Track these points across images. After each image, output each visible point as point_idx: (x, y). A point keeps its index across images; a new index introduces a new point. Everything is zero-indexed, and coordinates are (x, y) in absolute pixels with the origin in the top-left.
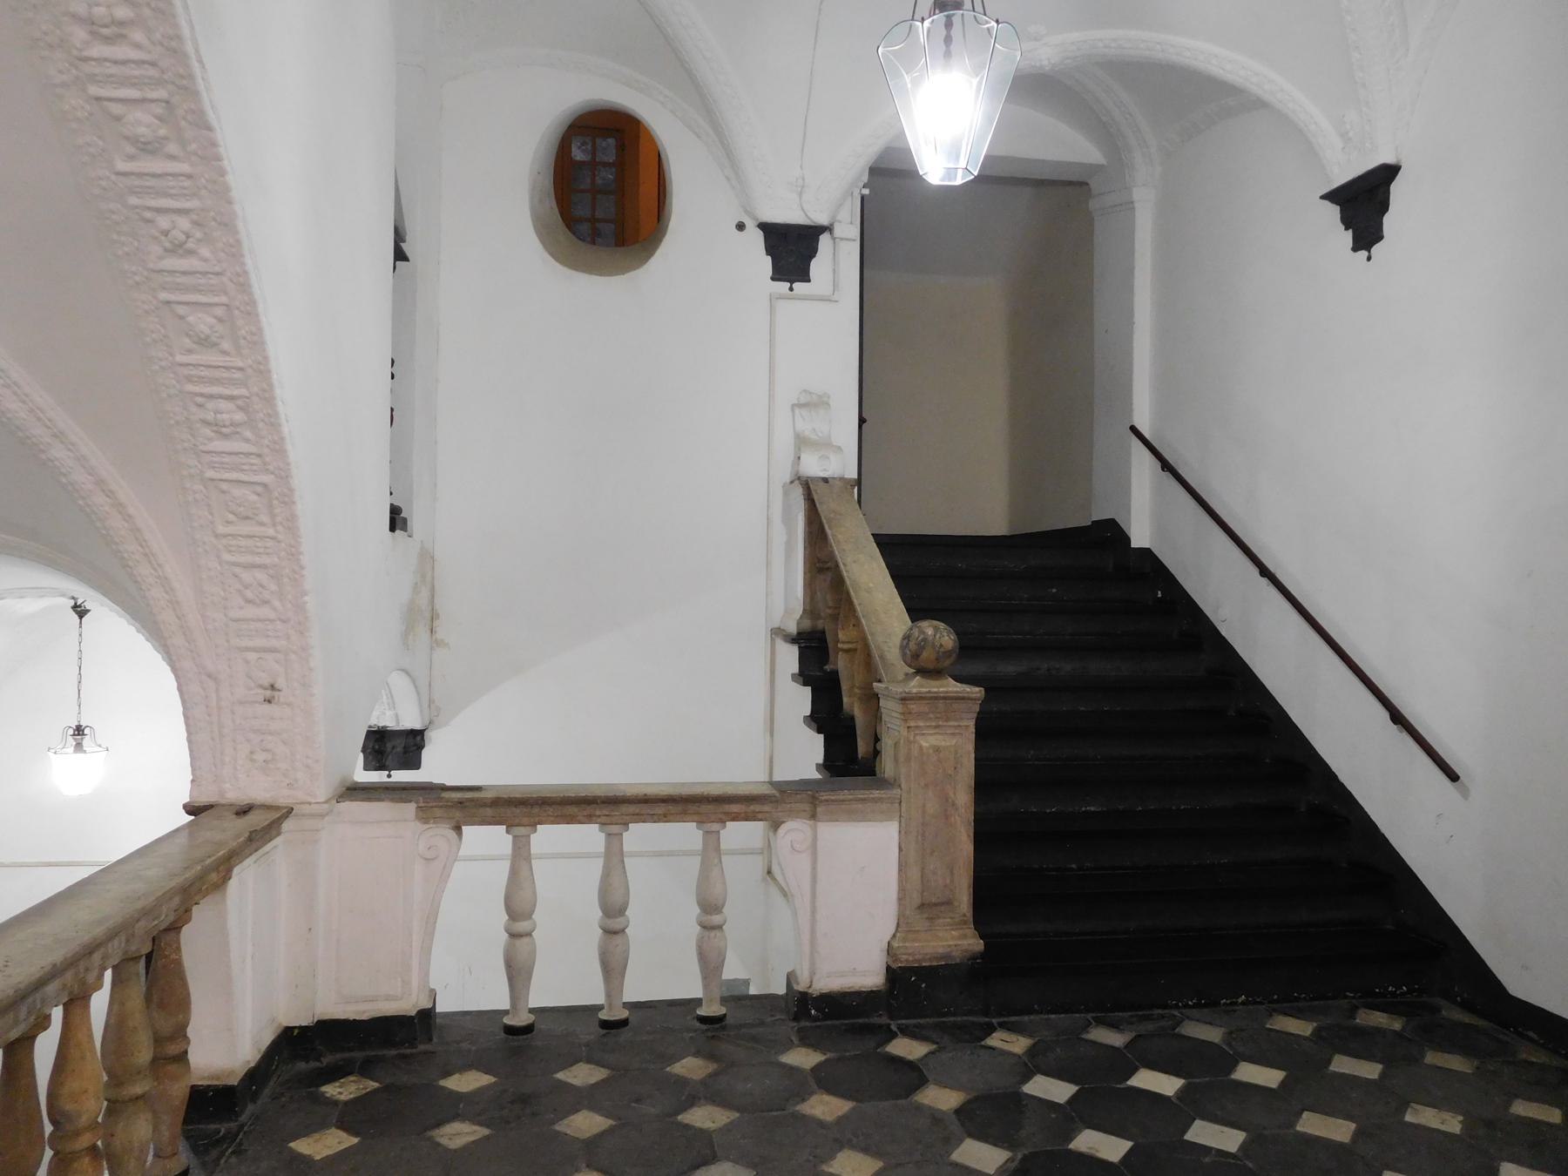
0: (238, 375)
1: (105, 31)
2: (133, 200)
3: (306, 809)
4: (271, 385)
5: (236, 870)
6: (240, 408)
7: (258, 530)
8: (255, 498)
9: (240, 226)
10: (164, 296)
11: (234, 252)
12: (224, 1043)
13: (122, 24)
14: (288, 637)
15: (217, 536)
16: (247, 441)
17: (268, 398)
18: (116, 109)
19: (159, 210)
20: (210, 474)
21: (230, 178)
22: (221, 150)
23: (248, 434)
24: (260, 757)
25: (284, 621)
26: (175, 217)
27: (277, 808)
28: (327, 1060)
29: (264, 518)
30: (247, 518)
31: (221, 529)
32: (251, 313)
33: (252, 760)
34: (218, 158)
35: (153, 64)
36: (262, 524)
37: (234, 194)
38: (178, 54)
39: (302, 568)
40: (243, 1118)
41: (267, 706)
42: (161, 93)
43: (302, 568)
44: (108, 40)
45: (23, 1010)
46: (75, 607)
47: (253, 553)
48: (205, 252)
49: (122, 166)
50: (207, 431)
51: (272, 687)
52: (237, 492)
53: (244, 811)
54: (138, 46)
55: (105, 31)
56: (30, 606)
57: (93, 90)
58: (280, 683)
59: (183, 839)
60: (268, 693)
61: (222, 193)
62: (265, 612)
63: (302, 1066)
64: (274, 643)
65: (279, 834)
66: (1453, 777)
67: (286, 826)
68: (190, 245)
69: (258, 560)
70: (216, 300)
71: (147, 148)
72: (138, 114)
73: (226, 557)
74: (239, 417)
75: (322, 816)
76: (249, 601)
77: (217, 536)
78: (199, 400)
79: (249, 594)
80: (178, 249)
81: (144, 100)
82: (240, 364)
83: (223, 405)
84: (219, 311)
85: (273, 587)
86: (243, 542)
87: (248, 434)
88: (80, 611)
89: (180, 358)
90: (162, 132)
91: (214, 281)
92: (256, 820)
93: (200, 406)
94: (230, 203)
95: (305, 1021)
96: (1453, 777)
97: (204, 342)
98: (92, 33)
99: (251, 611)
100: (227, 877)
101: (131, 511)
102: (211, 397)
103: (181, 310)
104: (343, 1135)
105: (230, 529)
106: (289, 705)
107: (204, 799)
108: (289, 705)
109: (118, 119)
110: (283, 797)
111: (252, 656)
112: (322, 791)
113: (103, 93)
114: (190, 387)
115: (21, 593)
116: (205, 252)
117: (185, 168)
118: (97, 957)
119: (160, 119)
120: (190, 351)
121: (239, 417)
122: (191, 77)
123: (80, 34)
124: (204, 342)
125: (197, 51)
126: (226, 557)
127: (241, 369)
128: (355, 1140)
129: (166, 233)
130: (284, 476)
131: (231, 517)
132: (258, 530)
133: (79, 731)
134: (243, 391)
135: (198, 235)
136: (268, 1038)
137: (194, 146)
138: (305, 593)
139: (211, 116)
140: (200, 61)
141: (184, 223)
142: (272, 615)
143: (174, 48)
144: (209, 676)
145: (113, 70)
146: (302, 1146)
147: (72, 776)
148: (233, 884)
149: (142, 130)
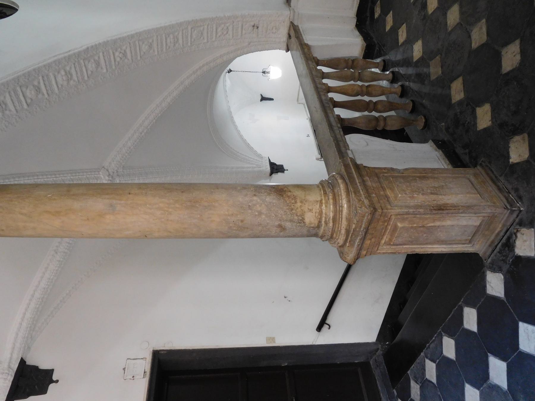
0: (159, 37)
1: (69, 76)
2: (114, 67)
3: (291, 17)
4: (161, 27)
5: (306, 42)
6: (169, 36)
7: (205, 31)
8: (195, 31)
9: (114, 38)
10: (139, 58)
11: (123, 39)
12: (352, 45)
13: (66, 72)
14: (238, 21)
15: (208, 42)
16: (178, 34)
17: (165, 28)
18: (89, 73)
19: (115, 61)
20: (189, 44)
21: (101, 41)
22: (93, 44)
23: (176, 33)
24: (274, 31)
25: (233, 22)
26: (116, 56)
27: (290, 26)
28: (368, 14)
29: (202, 28)
30: (202, 33)
31: (206, 41)
32: (139, 34)
33: (275, 33)
34: (96, 45)
35: (74, 64)
36: (204, 29)
37: (105, 40)
38: (70, 57)
39: (217, 17)
40: (376, 42)
41: (260, 28)
42: (82, 61)
43: (217, 17)
44: (71, 75)
45: (326, 105)
46: (228, 72)
47: (213, 32)
48: (124, 48)
49: (105, 71)
50: (177, 45)
51: (253, 26)
52: (194, 37)
53: (290, 37)
54: (71, 68)
55: (69, 76)
56: (228, 83)
57: (86, 78)
58: (252, 24)
59: (294, 52)
60: (255, 27)
61: (105, 44)
62: (230, 28)
63: (368, 23)
64: (240, 25)
65: (298, 26)
66: (272, 99)
67: (296, 24)
68: (123, 52)
69: (215, 30)
70: (137, 44)
71: (98, 64)
72: (89, 66)
73: (214, 39)
74: (171, 36)
75: (294, 12)
76: (227, 33)
77: (208, 42)
78: (168, 47)
79: (225, 33)
80: (125, 54)
81: (85, 66)
82: (156, 37)
83: (168, 41)
84: (141, 43)
85: (223, 25)
86: (209, 35)
87: (176, 33)
88: (230, 71)
89: (156, 53)
90: (93, 61)
91: (132, 44)
92: (293, 33)
93: (169, 48)
94: (108, 41)
95: (355, 20)
96: (272, 99)
97: (151, 46)
98: (71, 79)
99: (230, 32)
100: (307, 45)
101: (201, 65)
102: (166, 44)
103: (142, 53)
104: (389, 16)
105: (206, 38)
106: (259, 21)
107: (285, 47)
108: (259, 21)
109: (92, 72)
110: (287, 24)
111: (244, 32)
112: (286, 12)
113: (86, 76)
114: (164, 50)
115: (225, 86)
116: (124, 48)
117: (101, 54)
118: (319, 86)
119: (89, 61)
120: (154, 51)
121: (171, 36)
122: (74, 54)
123: (72, 82)
124: (151, 46)
125: (67, 52)
126: (214, 39)
127: (157, 36)
128: (391, 12)
129: (121, 58)
130: (189, 23)
131: (202, 38)
132: (205, 31)
133: (264, 72)
134: (164, 35)
135: (119, 50)
136: (357, 33)
137: (94, 52)
138: (225, 16)
139: (84, 48)
140: (69, 51)
141: (117, 54)
142: (231, 26)
143: (69, 58)
144: (249, 44)
145: (79, 74)
146: (388, 28)
147: (276, 73)
148: (309, 43)
149: (93, 65)
